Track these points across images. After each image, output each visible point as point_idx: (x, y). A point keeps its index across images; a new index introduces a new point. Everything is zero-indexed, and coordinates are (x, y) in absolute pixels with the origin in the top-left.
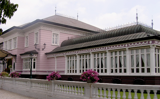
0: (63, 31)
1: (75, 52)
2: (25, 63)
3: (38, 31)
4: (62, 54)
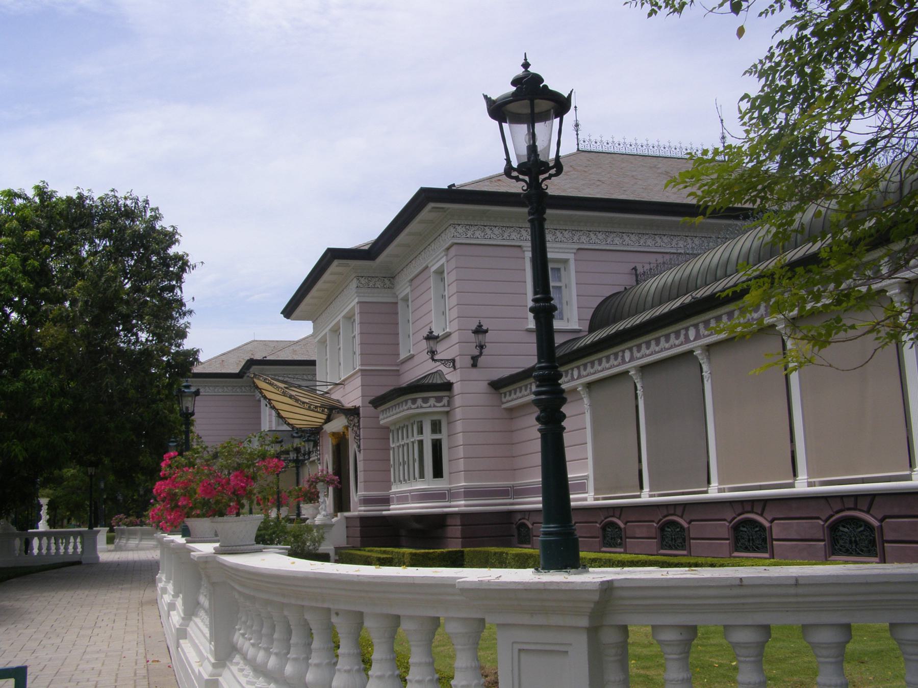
0: (598, 241)
1: (683, 332)
2: (410, 445)
3: (444, 260)
4: (677, 337)
